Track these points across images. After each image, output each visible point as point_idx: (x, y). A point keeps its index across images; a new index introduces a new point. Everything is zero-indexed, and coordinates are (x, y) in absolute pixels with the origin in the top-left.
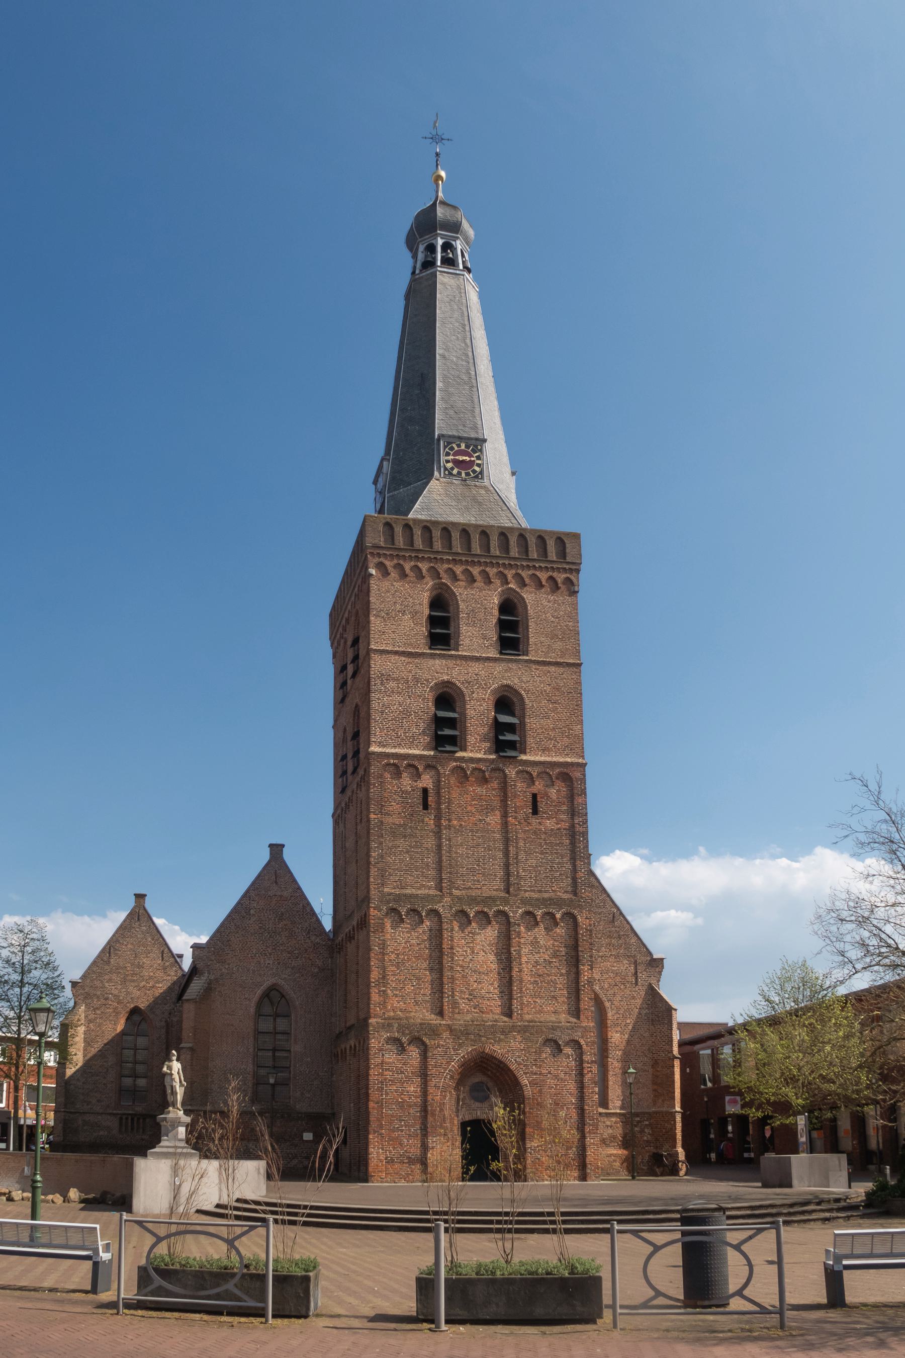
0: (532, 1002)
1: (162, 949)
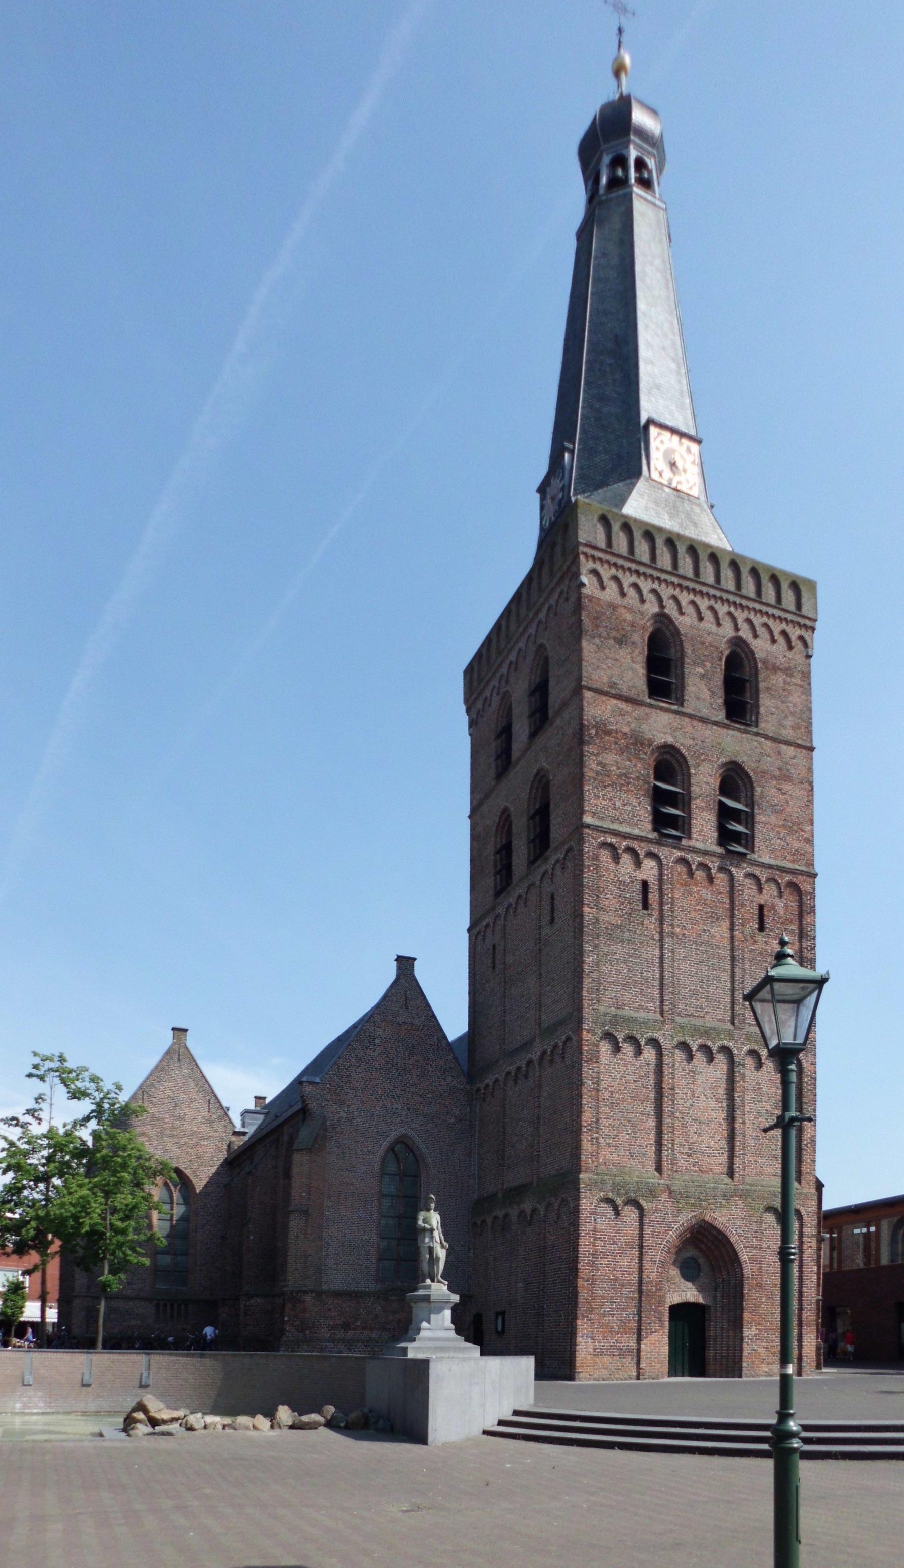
0: (753, 1162)
1: (208, 1098)
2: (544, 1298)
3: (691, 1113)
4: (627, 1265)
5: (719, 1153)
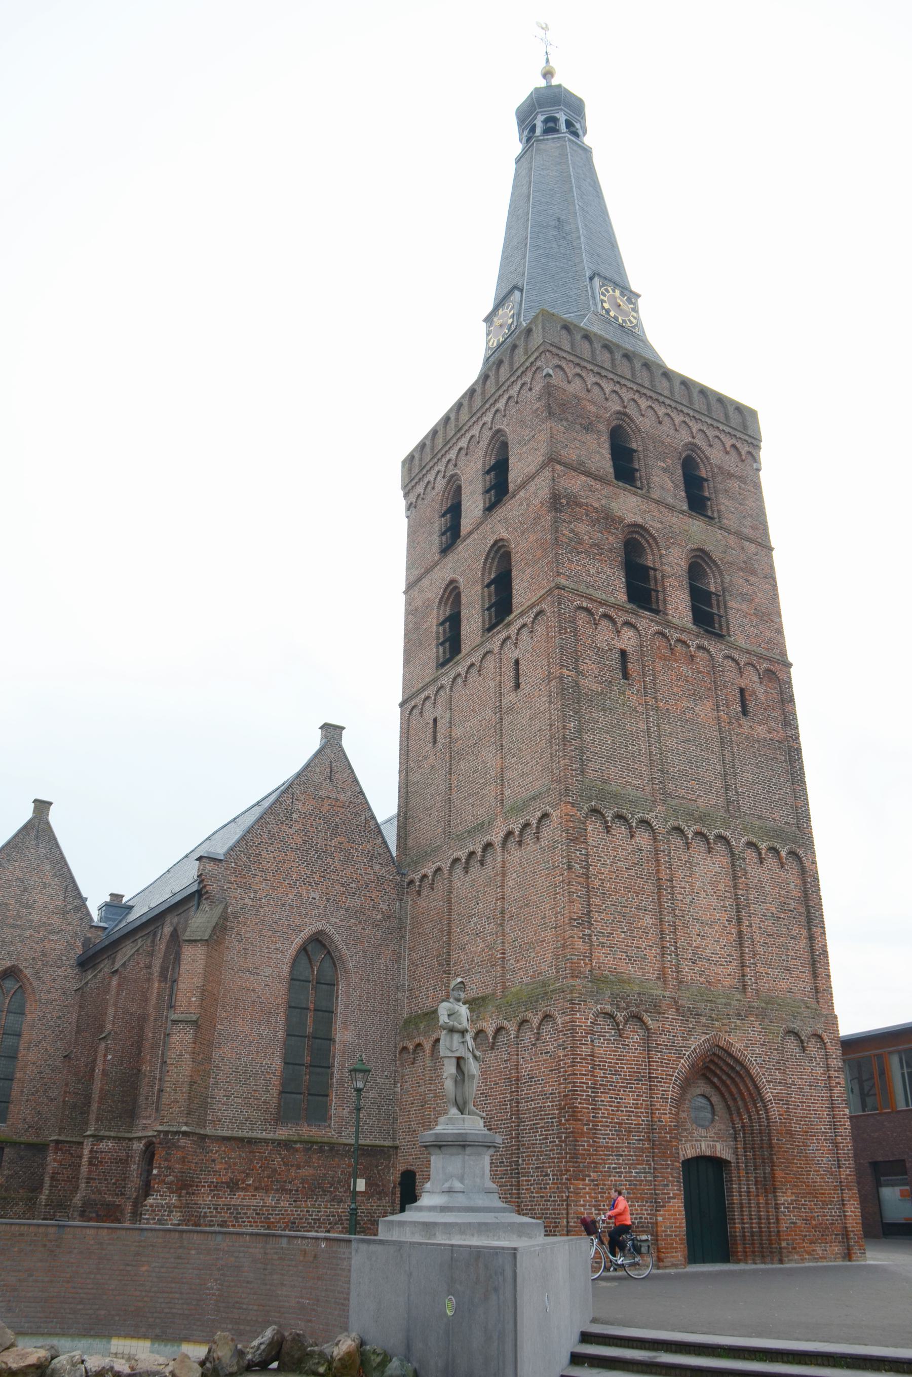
2: (519, 1149)
3: (691, 910)
4: (633, 1104)
5: (726, 962)
